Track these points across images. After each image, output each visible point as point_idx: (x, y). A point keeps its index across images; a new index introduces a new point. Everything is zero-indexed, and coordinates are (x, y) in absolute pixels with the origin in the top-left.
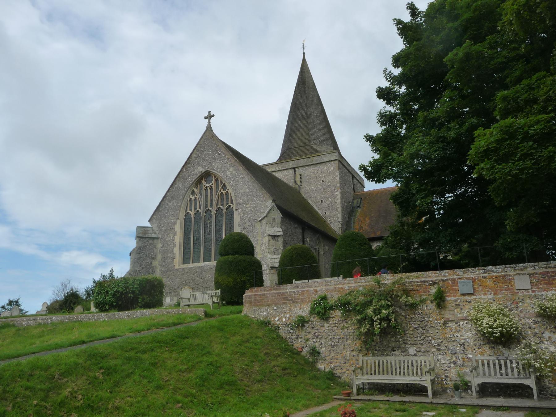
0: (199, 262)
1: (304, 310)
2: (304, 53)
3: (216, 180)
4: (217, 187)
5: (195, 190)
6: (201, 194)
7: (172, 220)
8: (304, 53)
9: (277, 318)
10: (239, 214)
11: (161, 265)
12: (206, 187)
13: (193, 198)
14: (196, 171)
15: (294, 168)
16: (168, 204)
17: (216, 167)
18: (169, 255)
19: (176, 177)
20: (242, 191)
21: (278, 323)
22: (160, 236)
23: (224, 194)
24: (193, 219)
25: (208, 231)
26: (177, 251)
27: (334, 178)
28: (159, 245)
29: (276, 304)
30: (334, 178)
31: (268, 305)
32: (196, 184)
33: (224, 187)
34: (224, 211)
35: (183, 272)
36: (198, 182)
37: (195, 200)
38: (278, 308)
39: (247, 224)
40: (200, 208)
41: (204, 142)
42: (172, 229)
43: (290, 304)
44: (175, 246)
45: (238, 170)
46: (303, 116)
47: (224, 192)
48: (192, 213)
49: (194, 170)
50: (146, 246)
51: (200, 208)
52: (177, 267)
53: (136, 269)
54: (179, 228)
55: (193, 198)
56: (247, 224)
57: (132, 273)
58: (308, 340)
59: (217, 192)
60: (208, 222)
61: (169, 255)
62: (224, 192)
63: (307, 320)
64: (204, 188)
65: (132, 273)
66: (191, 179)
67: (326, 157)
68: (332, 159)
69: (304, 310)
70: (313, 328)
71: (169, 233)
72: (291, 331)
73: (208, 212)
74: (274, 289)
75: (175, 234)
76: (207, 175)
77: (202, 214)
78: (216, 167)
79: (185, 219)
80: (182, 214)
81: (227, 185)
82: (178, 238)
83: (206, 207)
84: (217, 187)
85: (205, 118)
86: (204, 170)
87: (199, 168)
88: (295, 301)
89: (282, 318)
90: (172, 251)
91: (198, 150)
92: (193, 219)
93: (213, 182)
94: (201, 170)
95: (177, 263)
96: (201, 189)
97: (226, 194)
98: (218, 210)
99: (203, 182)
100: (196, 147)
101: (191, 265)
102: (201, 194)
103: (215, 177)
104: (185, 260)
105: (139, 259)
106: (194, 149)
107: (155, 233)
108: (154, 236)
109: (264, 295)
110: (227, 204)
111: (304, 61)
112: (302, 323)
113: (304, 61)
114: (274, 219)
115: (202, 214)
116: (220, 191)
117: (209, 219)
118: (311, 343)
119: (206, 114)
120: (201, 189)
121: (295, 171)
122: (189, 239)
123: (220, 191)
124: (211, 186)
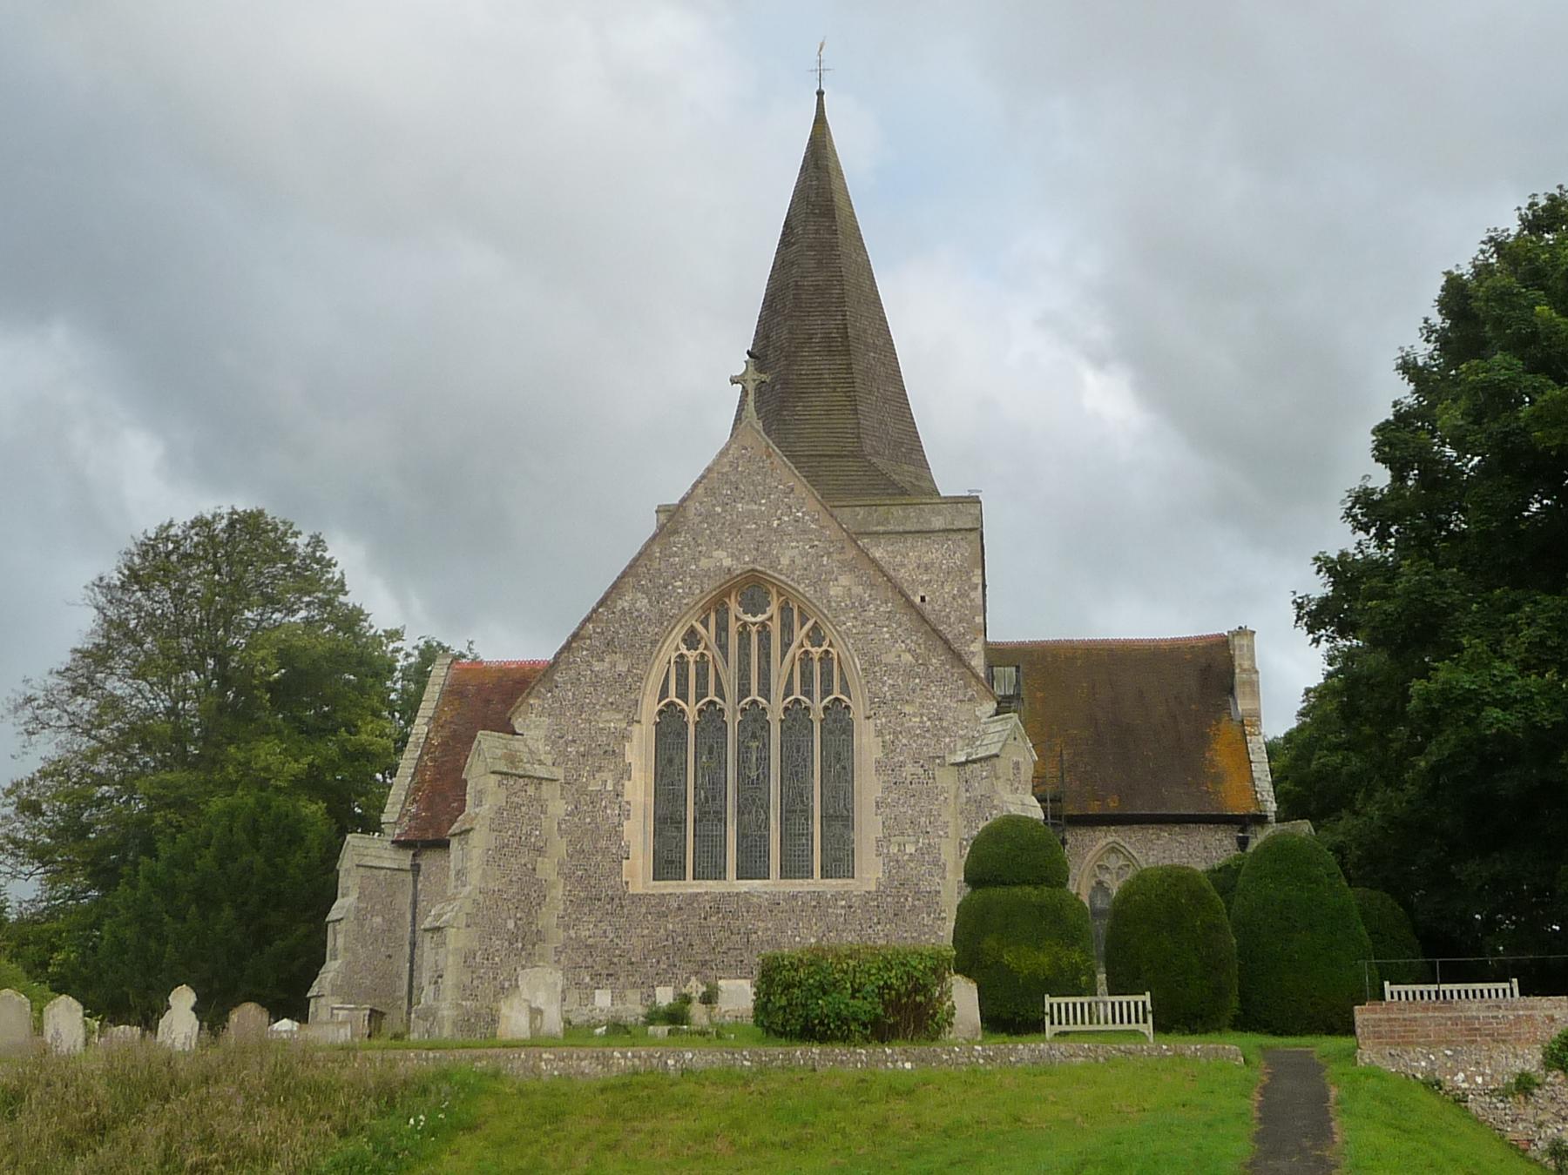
0: (720, 874)
1: (1530, 1060)
2: (820, 94)
3: (785, 610)
4: (787, 627)
5: (700, 627)
6: (723, 647)
7: (612, 721)
8: (820, 94)
9: (1461, 1076)
10: (879, 733)
11: (567, 877)
12: (745, 625)
13: (692, 656)
14: (704, 563)
16: (590, 665)
17: (785, 561)
18: (603, 843)
19: (624, 575)
20: (890, 658)
21: (1465, 1085)
22: (559, 773)
23: (816, 657)
24: (691, 729)
25: (753, 775)
26: (638, 835)
27: (963, 594)
28: (558, 807)
29: (1449, 1044)
30: (963, 594)
31: (1430, 1045)
32: (706, 610)
33: (816, 636)
34: (817, 714)
35: (660, 908)
36: (718, 606)
37: (702, 664)
38: (1455, 1051)
39: (910, 768)
40: (720, 692)
41: (734, 465)
43: (1486, 1043)
45: (872, 586)
46: (827, 337)
47: (816, 652)
48: (691, 711)
49: (696, 560)
50: (519, 806)
51: (720, 692)
52: (637, 888)
53: (491, 886)
54: (639, 753)
55: (692, 656)
56: (910, 768)
57: (480, 898)
58: (1540, 1125)
59: (786, 646)
60: (754, 744)
61: (603, 843)
62: (816, 652)
63: (1538, 1081)
64: (733, 627)
65: (480, 898)
66: (689, 593)
67: (939, 513)
68: (958, 524)
69: (1530, 1060)
70: (1552, 1099)
71: (600, 769)
72: (1500, 1105)
73: (755, 719)
74: (1435, 1009)
75: (625, 773)
76: (753, 588)
77: (732, 719)
78: (785, 561)
79: (657, 724)
80: (650, 708)
81: (828, 630)
82: (639, 790)
83: (744, 691)
84: (787, 627)
85: (733, 382)
86: (738, 568)
87: (715, 554)
88: (1498, 1039)
89: (1473, 1075)
90: (616, 833)
91: (711, 492)
92: (691, 729)
93: (773, 609)
94: (727, 562)
95: (638, 873)
96: (722, 628)
97: (821, 659)
98: (796, 715)
100: (703, 477)
101: (690, 886)
102: (723, 647)
103: (780, 594)
104: (667, 866)
105: (499, 849)
106: (695, 486)
107: (541, 762)
108: (541, 772)
109: (1415, 1020)
110: (826, 692)
111: (820, 120)
112: (1525, 1085)
113: (820, 120)
114: (1017, 765)
115: (732, 719)
116: (802, 645)
117: (754, 736)
118: (1551, 1131)
120: (722, 628)
122: (679, 798)
123: (802, 645)
124: (763, 624)
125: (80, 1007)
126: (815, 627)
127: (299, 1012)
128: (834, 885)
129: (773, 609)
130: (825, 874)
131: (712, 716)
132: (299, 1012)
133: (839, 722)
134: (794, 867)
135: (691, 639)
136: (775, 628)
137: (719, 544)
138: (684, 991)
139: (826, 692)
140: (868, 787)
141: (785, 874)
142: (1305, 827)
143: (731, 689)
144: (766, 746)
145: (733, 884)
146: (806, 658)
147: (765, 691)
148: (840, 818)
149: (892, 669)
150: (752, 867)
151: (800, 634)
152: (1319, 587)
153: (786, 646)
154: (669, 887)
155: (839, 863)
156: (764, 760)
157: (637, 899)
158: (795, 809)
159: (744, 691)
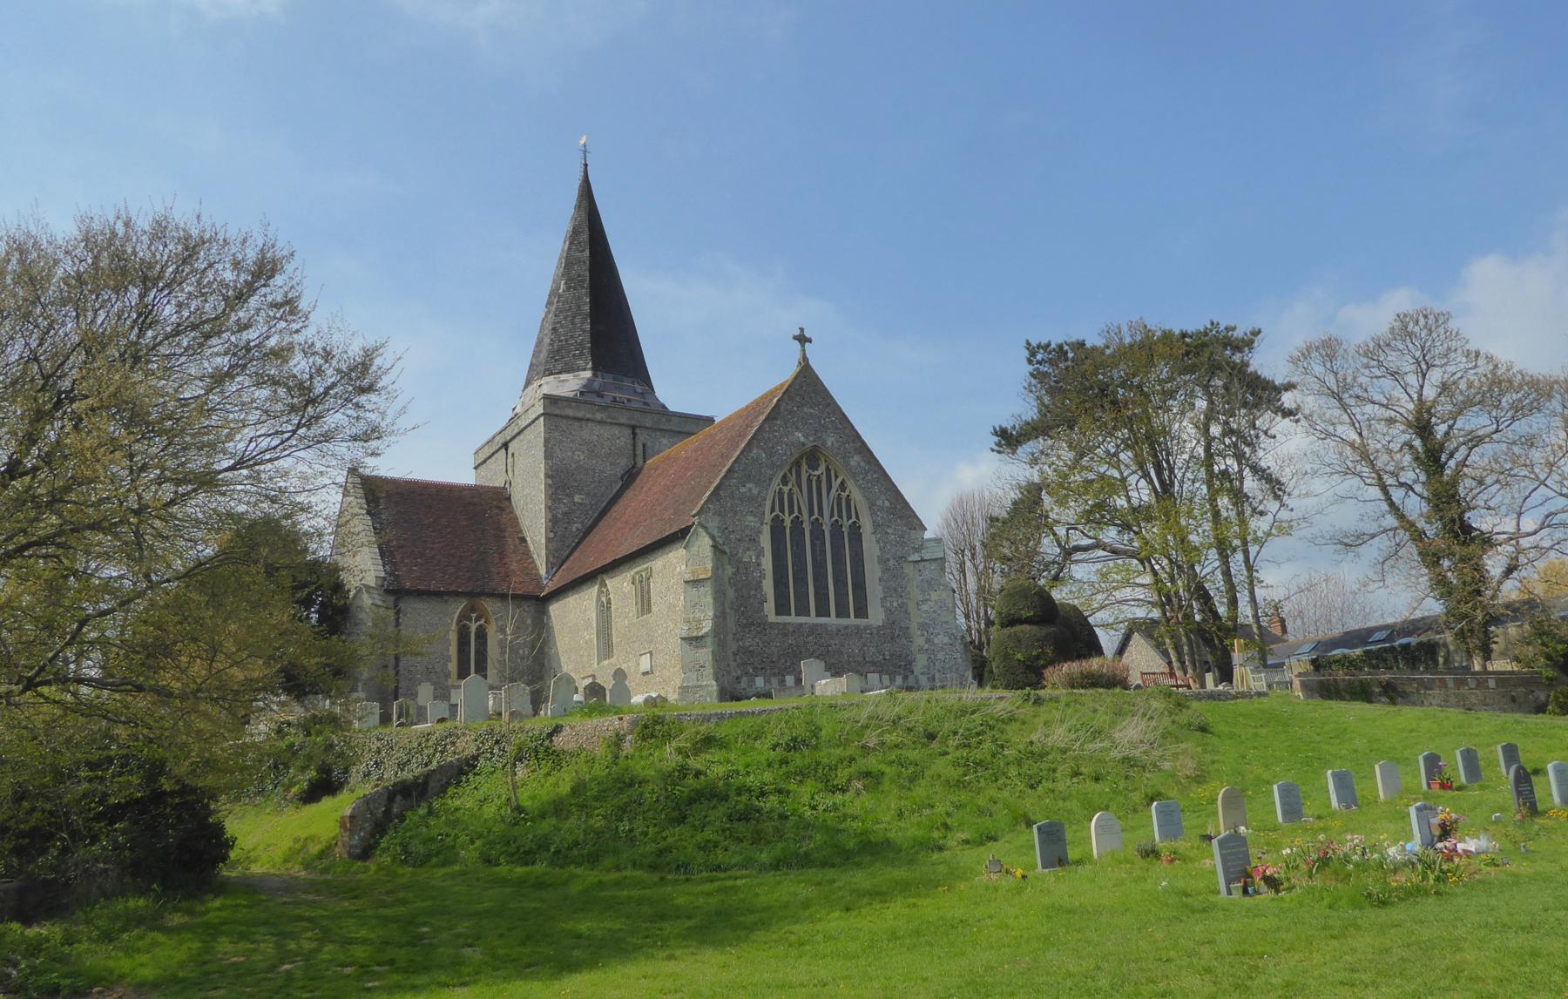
3: (828, 469)
7: (751, 521)
15: (633, 428)
20: (879, 503)
34: (788, 523)
36: (797, 464)
40: (800, 511)
42: (754, 540)
44: (763, 576)
64: (804, 477)
73: (817, 526)
75: (760, 553)
82: (767, 563)
90: (759, 587)
93: (822, 469)
98: (836, 528)
99: (804, 467)
104: (782, 608)
119: (798, 333)
120: (799, 476)
121: (634, 434)
126: (843, 483)
128: (859, 622)
129: (822, 469)
130: (838, 616)
131: (797, 522)
134: (803, 610)
135: (785, 481)
136: (824, 478)
137: (797, 429)
138: (624, 666)
139: (849, 518)
140: (873, 572)
141: (838, 616)
144: (824, 543)
145: (852, 620)
146: (781, 492)
148: (860, 586)
150: (822, 611)
151: (836, 484)
155: (862, 612)
157: (772, 625)
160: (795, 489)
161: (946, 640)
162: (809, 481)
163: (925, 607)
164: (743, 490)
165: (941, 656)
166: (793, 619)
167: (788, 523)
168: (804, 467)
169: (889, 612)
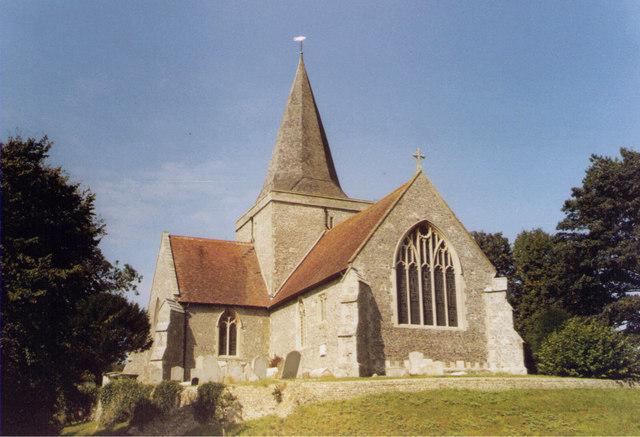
20: (466, 255)
33: (442, 245)
34: (407, 267)
51: (441, 263)
59: (434, 247)
73: (425, 269)
83: (446, 264)
94: (418, 217)
98: (438, 270)
99: (419, 234)
110: (446, 264)
125: (511, 308)
127: (456, 325)
129: (429, 234)
131: (413, 268)
132: (456, 325)
133: (450, 271)
136: (431, 241)
142: (575, 198)
143: (418, 260)
147: (428, 262)
148: (452, 307)
149: (467, 259)
150: (428, 321)
151: (438, 245)
152: (572, 192)
153: (434, 247)
154: (403, 325)
155: (453, 322)
156: (429, 285)
158: (439, 304)
159: (422, 261)
160: (413, 246)
161: (508, 341)
162: (421, 242)
163: (495, 321)
164: (380, 247)
165: (504, 351)
166: (409, 326)
167: (407, 267)
168: (419, 234)
169: (471, 323)
